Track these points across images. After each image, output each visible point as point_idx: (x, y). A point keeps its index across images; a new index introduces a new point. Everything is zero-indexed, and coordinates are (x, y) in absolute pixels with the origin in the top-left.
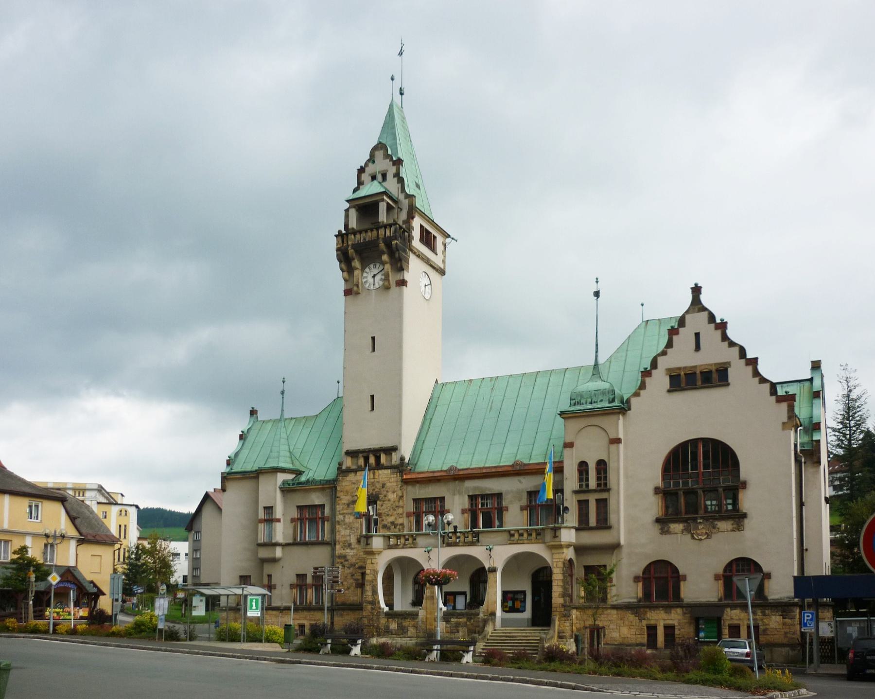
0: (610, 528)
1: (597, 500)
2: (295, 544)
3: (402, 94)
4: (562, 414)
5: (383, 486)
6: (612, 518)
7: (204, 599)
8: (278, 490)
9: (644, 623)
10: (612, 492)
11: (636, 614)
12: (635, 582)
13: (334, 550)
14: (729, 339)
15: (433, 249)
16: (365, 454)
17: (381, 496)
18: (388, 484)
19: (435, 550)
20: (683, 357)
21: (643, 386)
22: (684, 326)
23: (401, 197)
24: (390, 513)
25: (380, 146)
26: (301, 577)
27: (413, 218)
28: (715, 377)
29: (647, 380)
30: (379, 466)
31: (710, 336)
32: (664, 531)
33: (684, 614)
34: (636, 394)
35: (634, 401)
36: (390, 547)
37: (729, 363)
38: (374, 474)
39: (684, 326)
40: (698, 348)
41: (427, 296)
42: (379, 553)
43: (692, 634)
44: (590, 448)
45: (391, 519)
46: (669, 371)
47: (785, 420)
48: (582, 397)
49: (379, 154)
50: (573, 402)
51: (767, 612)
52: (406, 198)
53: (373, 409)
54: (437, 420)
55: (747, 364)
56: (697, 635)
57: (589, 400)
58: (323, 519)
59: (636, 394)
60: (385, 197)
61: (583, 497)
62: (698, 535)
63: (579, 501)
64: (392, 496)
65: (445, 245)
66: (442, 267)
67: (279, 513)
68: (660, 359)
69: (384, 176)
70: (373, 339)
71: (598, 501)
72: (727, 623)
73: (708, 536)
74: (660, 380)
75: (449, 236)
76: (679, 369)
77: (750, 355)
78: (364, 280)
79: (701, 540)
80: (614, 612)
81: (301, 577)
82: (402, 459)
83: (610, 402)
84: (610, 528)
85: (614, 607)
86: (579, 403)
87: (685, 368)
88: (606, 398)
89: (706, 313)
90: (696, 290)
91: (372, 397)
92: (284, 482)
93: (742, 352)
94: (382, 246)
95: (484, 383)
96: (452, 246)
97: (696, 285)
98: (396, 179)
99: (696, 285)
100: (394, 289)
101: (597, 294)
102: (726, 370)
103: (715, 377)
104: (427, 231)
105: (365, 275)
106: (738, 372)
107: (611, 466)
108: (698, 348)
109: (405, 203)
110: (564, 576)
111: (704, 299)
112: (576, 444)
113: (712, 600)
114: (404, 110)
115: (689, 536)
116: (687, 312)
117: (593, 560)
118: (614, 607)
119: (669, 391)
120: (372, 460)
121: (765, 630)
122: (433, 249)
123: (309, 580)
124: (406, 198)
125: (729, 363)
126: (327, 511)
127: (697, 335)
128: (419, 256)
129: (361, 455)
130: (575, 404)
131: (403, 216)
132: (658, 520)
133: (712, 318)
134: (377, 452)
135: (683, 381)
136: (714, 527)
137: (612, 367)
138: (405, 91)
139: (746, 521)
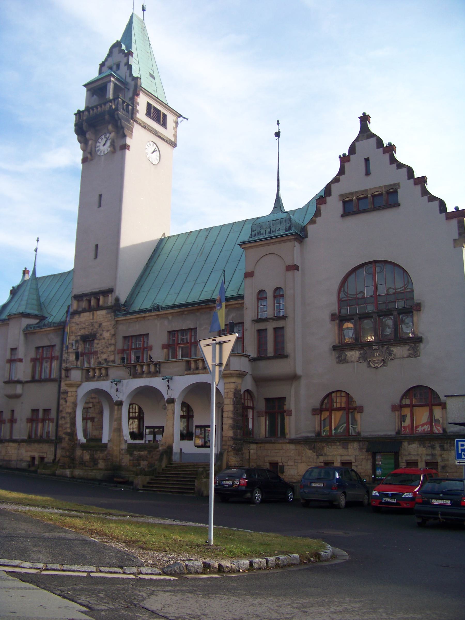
0: (287, 357)
1: (275, 329)
2: (33, 380)
3: (144, 10)
4: (242, 244)
5: (100, 325)
6: (289, 348)
7: (393, 453)
8: (22, 332)
9: (321, 459)
10: (289, 320)
11: (313, 449)
12: (313, 414)
13: (60, 386)
14: (397, 161)
15: (164, 125)
16: (88, 298)
17: (98, 335)
18: (104, 324)
19: (124, 382)
20: (357, 183)
21: (318, 213)
22: (355, 153)
23: (129, 80)
24: (104, 351)
25: (117, 45)
26: (35, 411)
27: (138, 95)
28: (387, 199)
29: (322, 207)
30: (99, 308)
31: (378, 159)
32: (341, 360)
33: (361, 449)
34: (312, 222)
35: (310, 229)
36: (88, 379)
37: (398, 185)
38: (93, 314)
39: (355, 153)
40: (368, 173)
41: (155, 162)
42: (79, 386)
43: (370, 471)
44: (268, 279)
45: (104, 356)
46: (341, 196)
47: (456, 236)
48: (261, 227)
49: (116, 50)
50: (253, 233)
51: (446, 446)
52: (132, 80)
53: (96, 256)
54: (157, 267)
55: (415, 184)
56: (374, 472)
57: (268, 230)
58: (52, 359)
59: (312, 222)
60: (112, 79)
61: (261, 326)
62: (374, 362)
63: (259, 331)
64: (106, 335)
65: (177, 123)
66: (173, 139)
67: (21, 354)
68: (333, 187)
69: (118, 66)
70: (100, 196)
71: (276, 330)
72: (405, 458)
73: (385, 363)
74: (334, 206)
75: (180, 116)
76: (352, 194)
77: (417, 175)
78: (97, 149)
79: (377, 368)
80: (292, 447)
81: (35, 411)
82: (117, 300)
83: (286, 231)
84: (287, 357)
85: (292, 441)
86: (259, 234)
87: (357, 192)
88: (283, 228)
89: (374, 139)
90: (365, 119)
91: (97, 246)
92: (28, 326)
93: (410, 171)
94: (107, 117)
95: (201, 233)
96: (183, 124)
97: (364, 114)
98: (126, 67)
99: (364, 114)
100: (119, 152)
101: (278, 134)
102: (396, 192)
103: (387, 199)
104: (155, 108)
105: (98, 144)
106: (406, 193)
107: (288, 292)
108: (368, 173)
109: (132, 83)
110: (235, 407)
111: (373, 127)
112: (256, 274)
113: (389, 433)
114: (145, 21)
115: (365, 364)
116: (357, 140)
117: (274, 392)
118: (292, 441)
119: (342, 216)
120: (93, 303)
121: (444, 467)
122: (164, 125)
123: (41, 415)
124: (132, 80)
125: (398, 185)
126: (56, 353)
127: (367, 160)
128: (145, 126)
129: (85, 298)
130: (255, 235)
131: (130, 94)
132: (335, 348)
133: (379, 142)
134: (96, 295)
135: (353, 206)
136: (390, 354)
137: (309, 210)
138: (147, 8)
139: (422, 345)
